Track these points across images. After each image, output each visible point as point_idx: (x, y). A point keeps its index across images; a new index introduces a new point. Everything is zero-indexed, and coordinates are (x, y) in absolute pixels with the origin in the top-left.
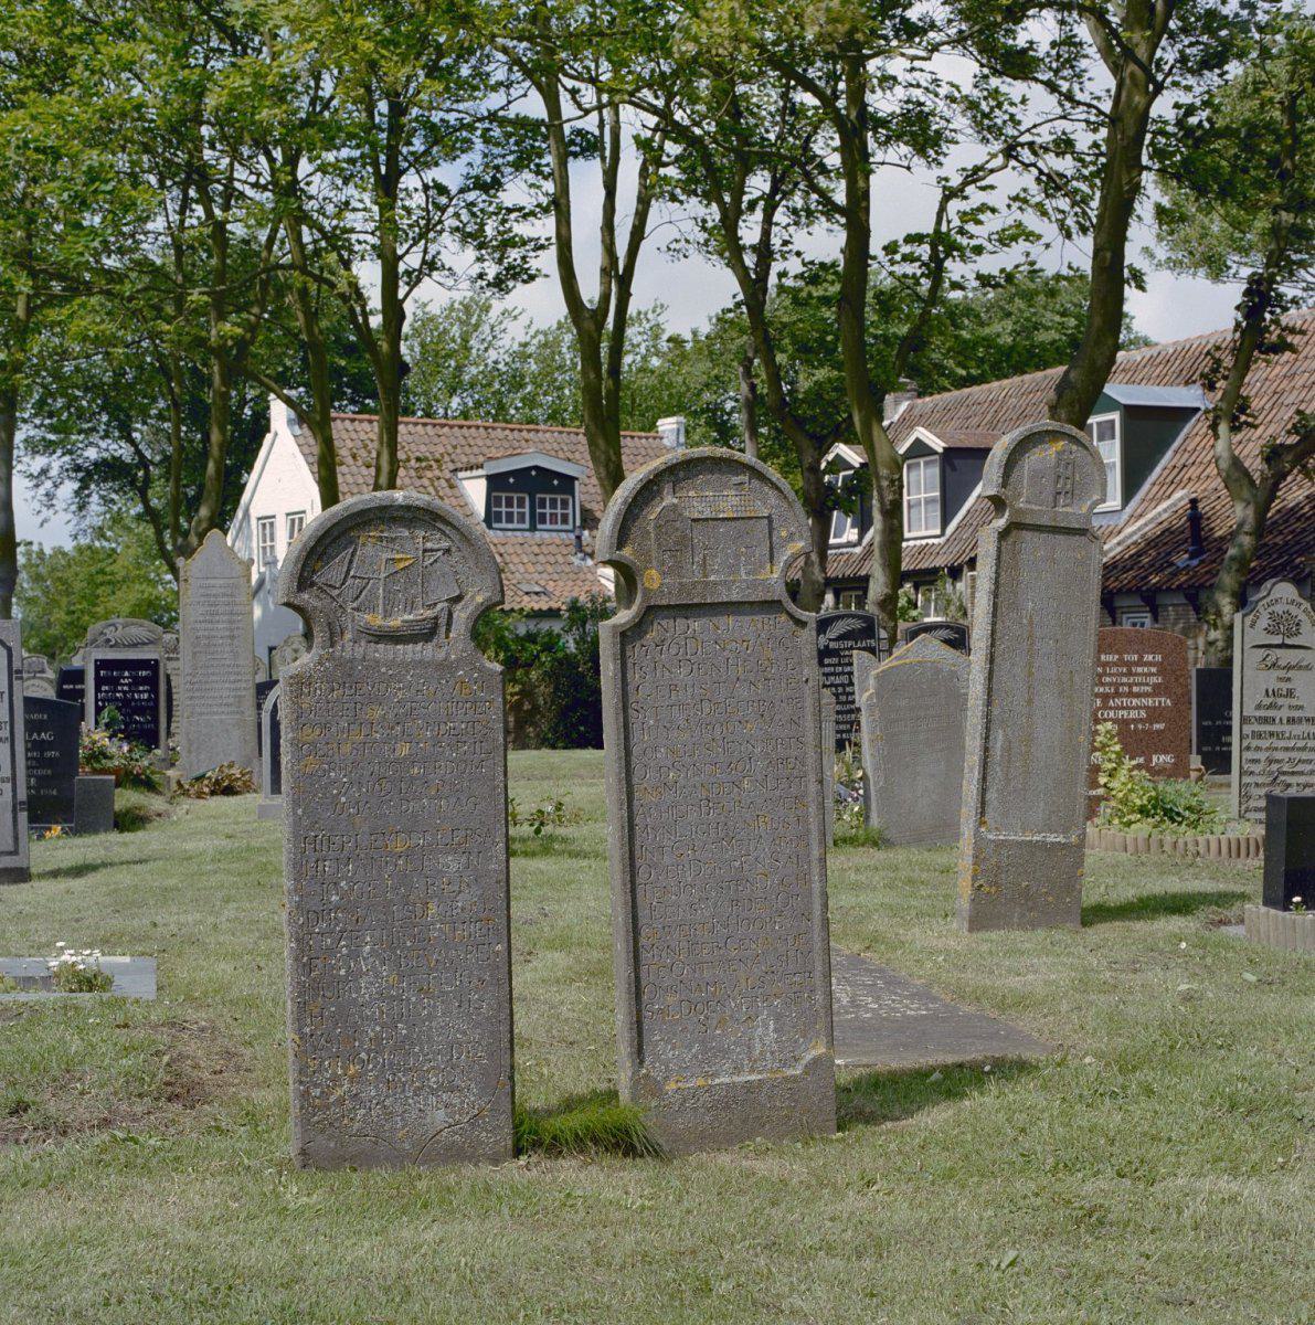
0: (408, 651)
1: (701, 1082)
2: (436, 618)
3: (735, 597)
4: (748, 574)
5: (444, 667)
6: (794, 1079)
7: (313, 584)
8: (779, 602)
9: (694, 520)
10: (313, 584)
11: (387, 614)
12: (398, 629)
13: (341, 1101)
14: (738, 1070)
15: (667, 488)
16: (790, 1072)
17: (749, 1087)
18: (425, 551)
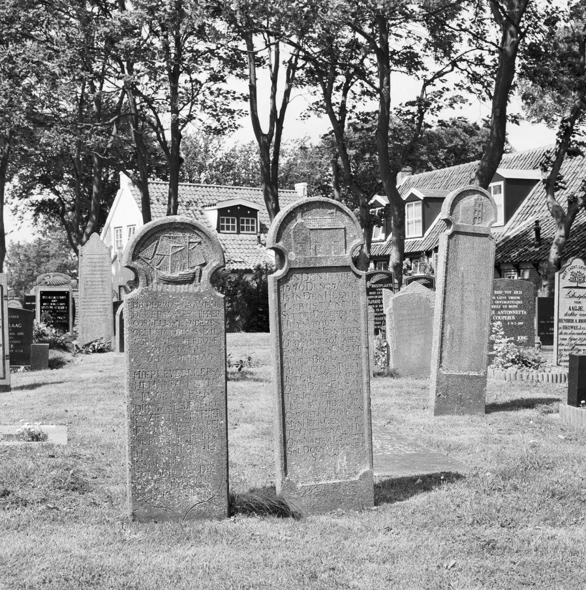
0: (182, 288)
1: (313, 483)
2: (194, 273)
3: (329, 264)
4: (335, 254)
5: (198, 295)
6: (355, 482)
7: (139, 258)
8: (349, 266)
9: (311, 230)
10: (139, 258)
11: (172, 271)
12: (177, 278)
13: (150, 491)
14: (329, 478)
15: (299, 215)
16: (353, 479)
17: (335, 486)
18: (190, 243)
